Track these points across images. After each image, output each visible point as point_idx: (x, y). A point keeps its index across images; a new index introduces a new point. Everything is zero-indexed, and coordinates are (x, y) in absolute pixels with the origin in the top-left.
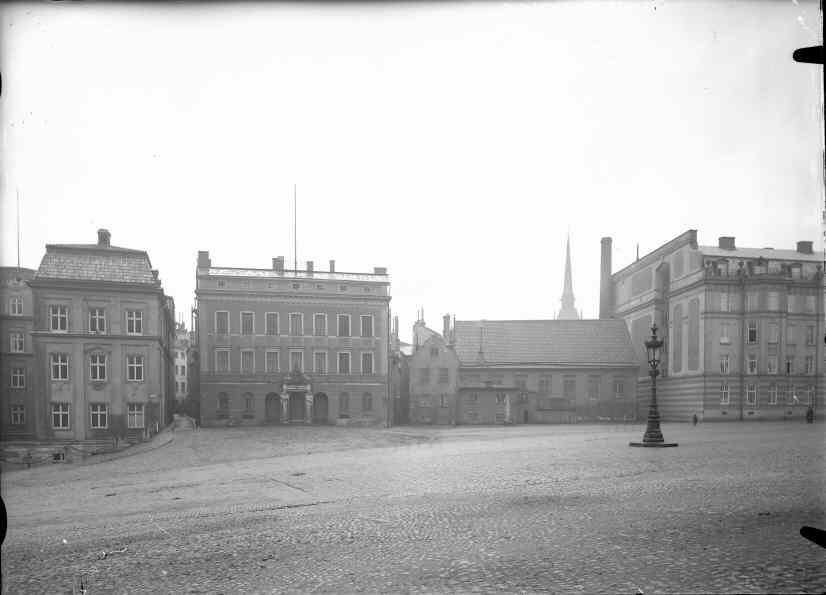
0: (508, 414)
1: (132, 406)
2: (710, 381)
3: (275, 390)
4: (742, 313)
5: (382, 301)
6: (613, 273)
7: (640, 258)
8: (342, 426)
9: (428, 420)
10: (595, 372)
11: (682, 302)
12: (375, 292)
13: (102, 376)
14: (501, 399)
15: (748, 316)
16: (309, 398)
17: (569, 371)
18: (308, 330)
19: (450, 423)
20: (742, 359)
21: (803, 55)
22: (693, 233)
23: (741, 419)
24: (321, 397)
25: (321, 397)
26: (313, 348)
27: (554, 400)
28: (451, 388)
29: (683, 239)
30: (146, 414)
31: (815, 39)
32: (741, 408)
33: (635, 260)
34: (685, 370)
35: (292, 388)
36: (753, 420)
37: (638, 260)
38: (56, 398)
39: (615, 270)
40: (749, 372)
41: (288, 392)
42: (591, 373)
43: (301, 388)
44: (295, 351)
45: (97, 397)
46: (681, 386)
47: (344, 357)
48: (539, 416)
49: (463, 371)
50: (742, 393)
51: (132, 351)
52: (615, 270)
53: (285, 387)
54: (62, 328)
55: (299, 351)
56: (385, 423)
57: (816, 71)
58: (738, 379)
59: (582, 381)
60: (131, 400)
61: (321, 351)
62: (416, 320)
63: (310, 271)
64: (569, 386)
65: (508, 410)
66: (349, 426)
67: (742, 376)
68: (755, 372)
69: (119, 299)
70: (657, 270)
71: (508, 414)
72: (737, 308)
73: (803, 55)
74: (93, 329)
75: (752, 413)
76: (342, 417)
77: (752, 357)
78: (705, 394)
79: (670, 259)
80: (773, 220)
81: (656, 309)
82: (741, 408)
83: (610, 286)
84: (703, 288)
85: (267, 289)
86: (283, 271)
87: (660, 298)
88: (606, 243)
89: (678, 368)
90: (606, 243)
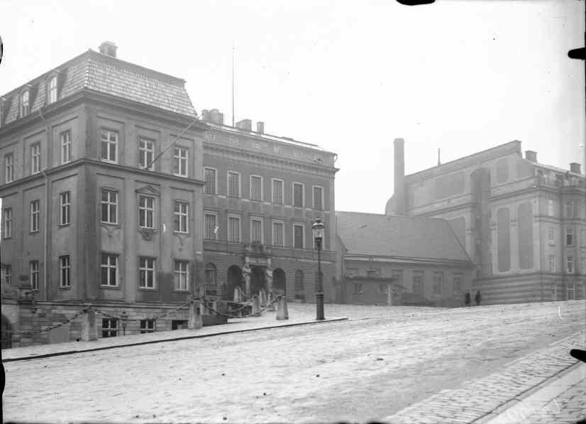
1: (177, 262)
2: (546, 279)
3: (237, 263)
5: (329, 172)
7: (442, 163)
13: (150, 224)
15: (566, 222)
16: (270, 273)
18: (267, 198)
20: (562, 260)
21: (574, 54)
24: (279, 274)
25: (279, 274)
26: (271, 218)
30: (192, 274)
31: (580, 44)
33: (436, 164)
34: (515, 268)
35: (253, 261)
38: (106, 247)
39: (407, 173)
41: (250, 266)
43: (261, 262)
44: (255, 218)
45: (148, 249)
46: (495, 286)
47: (299, 229)
51: (180, 195)
53: (247, 260)
54: (111, 159)
55: (213, 213)
57: (580, 63)
59: (429, 275)
60: (179, 256)
61: (279, 222)
63: (261, 131)
64: (418, 280)
67: (564, 275)
68: (573, 271)
69: (169, 132)
70: (471, 175)
73: (574, 54)
74: (142, 161)
75: (139, 363)
79: (491, 166)
80: (558, 151)
83: (406, 185)
84: (538, 193)
85: (268, 152)
86: (223, 125)
88: (399, 145)
89: (505, 265)
90: (399, 145)
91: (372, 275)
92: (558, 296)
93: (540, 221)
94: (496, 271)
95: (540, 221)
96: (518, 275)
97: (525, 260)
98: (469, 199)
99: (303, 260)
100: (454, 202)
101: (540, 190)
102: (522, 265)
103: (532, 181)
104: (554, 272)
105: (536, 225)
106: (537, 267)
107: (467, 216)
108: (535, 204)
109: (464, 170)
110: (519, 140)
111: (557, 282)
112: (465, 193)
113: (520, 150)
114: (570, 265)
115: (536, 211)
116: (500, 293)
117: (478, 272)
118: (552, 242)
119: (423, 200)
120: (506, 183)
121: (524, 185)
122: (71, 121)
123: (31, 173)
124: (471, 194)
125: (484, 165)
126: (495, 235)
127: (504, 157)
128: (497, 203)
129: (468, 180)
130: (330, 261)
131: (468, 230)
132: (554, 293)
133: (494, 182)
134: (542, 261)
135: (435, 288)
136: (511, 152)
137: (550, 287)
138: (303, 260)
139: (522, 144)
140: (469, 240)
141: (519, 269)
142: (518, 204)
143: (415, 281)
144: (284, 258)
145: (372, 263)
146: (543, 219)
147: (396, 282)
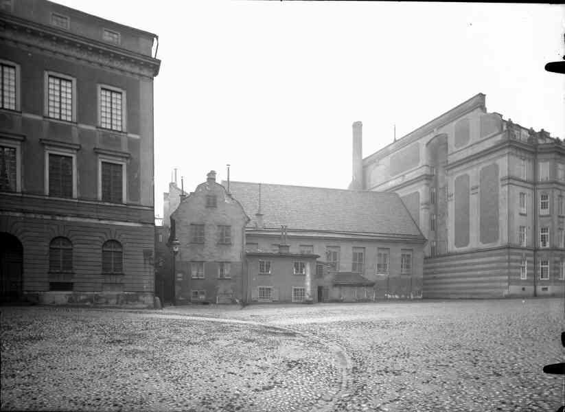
0: (308, 290)
4: (535, 183)
6: (363, 158)
7: (397, 139)
8: (55, 306)
9: (202, 297)
10: (385, 242)
11: (469, 172)
12: (129, 45)
14: (300, 268)
15: (540, 186)
17: (358, 240)
19: (234, 303)
21: (552, 67)
22: (482, 96)
23: (535, 295)
27: (340, 276)
28: (235, 253)
29: (470, 104)
32: (535, 283)
34: (475, 242)
36: (547, 296)
37: (395, 141)
40: (541, 247)
42: (381, 246)
48: (335, 293)
49: (251, 237)
50: (535, 269)
52: (366, 154)
56: (149, 299)
58: (532, 252)
59: (371, 252)
62: (170, 182)
64: (358, 259)
65: (308, 284)
66: (72, 304)
67: (536, 250)
70: (427, 144)
71: (308, 290)
72: (531, 178)
73: (552, 67)
75: (546, 289)
76: (55, 286)
77: (544, 230)
78: (509, 267)
79: (450, 130)
81: (427, 184)
82: (535, 283)
83: (364, 167)
87: (429, 173)
88: (358, 127)
89: (462, 238)
90: (358, 127)
91: (284, 251)
92: (118, 140)
93: (508, 184)
94: (451, 247)
95: (508, 184)
96: (478, 251)
97: (489, 227)
98: (424, 171)
99: (69, 219)
100: (409, 177)
101: (509, 146)
102: (483, 239)
103: (499, 138)
104: (525, 246)
105: (503, 190)
106: (503, 239)
107: (422, 190)
108: (504, 164)
109: (419, 141)
110: (484, 93)
111: (528, 258)
112: (420, 166)
113: (484, 106)
114: (543, 238)
115: (503, 172)
116: (441, 272)
117: (433, 249)
118: (524, 211)
119: (380, 179)
120: (468, 145)
121: (489, 144)
122: (230, 177)
123: (561, 281)
124: (426, 166)
125: (441, 131)
126: (451, 207)
127: (464, 117)
128: (454, 170)
129: (423, 151)
130: (139, 222)
131: (422, 204)
132: (524, 271)
133: (452, 147)
134: (510, 232)
135: (379, 266)
136: (472, 109)
137: (519, 264)
138: (69, 219)
139: (486, 97)
140: (423, 216)
141: (480, 243)
142: (480, 168)
143: (355, 259)
144: (49, 217)
145: (282, 237)
146: (511, 181)
147: (318, 259)
